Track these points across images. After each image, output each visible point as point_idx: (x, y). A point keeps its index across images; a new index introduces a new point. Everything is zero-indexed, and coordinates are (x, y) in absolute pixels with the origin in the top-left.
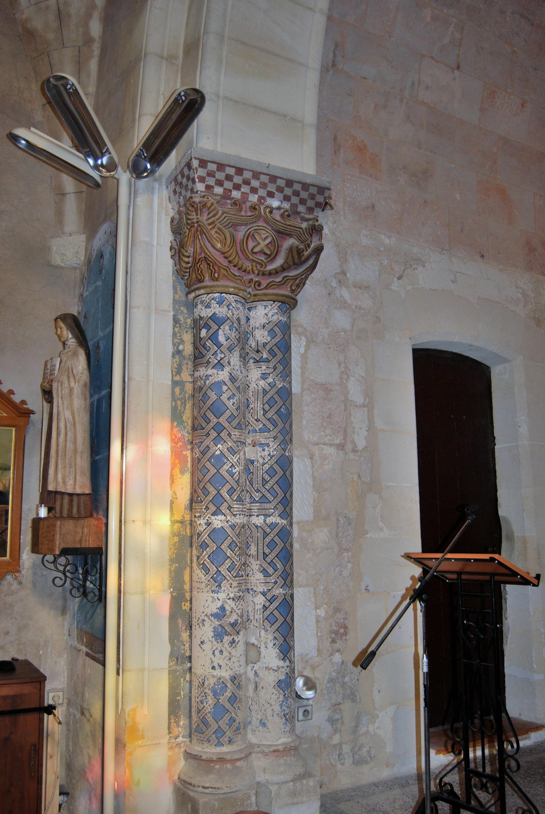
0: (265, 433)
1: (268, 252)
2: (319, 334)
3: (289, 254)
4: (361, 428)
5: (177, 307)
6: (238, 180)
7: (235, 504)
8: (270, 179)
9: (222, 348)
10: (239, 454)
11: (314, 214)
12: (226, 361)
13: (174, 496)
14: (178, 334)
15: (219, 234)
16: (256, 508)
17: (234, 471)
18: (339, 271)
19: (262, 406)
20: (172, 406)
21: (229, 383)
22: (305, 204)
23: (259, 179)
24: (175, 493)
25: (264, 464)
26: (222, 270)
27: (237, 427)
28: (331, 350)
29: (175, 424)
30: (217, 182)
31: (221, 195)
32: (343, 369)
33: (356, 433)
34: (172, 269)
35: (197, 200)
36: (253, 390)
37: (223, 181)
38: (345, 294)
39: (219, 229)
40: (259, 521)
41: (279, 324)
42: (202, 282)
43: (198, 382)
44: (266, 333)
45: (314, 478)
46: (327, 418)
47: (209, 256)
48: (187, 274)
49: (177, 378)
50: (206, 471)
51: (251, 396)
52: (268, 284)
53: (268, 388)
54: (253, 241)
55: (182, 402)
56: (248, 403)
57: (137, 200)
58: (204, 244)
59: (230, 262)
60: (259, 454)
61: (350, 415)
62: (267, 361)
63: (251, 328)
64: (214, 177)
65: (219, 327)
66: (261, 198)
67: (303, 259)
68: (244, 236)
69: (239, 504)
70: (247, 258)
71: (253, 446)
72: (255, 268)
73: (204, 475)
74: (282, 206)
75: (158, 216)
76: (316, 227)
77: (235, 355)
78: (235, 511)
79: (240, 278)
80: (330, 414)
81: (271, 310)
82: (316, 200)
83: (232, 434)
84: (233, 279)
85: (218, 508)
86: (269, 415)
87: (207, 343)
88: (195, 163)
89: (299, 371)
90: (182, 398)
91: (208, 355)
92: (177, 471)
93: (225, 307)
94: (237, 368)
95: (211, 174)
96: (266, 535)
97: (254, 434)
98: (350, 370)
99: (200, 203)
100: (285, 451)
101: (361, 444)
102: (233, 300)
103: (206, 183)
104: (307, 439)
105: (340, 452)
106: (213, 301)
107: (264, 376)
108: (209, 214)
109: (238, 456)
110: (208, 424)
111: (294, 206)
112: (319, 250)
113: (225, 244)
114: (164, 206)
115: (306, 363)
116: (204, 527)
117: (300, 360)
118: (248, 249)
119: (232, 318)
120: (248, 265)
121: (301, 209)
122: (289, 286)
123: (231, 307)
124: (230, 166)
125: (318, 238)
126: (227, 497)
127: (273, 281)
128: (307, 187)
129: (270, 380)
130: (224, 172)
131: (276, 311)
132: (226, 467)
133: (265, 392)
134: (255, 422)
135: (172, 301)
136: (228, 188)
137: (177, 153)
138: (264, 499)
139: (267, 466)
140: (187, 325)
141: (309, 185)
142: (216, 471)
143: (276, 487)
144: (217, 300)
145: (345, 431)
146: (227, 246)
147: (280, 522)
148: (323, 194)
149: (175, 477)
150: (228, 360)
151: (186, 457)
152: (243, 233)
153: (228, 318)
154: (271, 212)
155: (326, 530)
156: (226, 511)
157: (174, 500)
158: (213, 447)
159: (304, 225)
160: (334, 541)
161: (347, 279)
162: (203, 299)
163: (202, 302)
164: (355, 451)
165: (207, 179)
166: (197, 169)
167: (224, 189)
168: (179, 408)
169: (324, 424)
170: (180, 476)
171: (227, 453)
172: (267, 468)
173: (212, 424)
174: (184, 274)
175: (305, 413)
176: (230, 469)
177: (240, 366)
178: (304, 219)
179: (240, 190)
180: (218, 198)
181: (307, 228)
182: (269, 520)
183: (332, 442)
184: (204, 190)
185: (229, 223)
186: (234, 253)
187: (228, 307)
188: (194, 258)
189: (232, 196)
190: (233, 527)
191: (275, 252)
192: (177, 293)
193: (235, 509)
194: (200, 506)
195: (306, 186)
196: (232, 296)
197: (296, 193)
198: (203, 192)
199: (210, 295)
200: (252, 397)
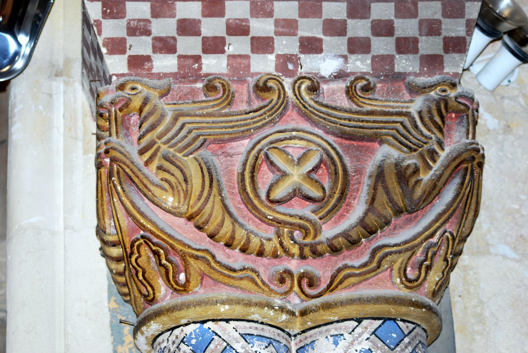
1: (316, 193)
11: (446, 70)
15: (168, 172)
22: (415, 50)
23: (270, 14)
26: (192, 261)
30: (158, 44)
31: (174, 75)
37: (174, 39)
39: (166, 158)
52: (333, 278)
54: (273, 172)
58: (132, 202)
64: (148, 33)
66: (285, 62)
67: (419, 192)
68: (245, 164)
70: (263, 218)
72: (287, 242)
74: (350, 68)
76: (452, 103)
81: (352, 343)
84: (226, 280)
102: (237, 335)
103: (129, 53)
106: (183, 347)
111: (383, 62)
118: (258, 196)
120: (264, 234)
121: (405, 64)
122: (395, 272)
125: (464, 130)
127: (346, 267)
130: (173, 16)
144: (193, 342)
148: (462, 16)
152: (240, 159)
159: (416, 105)
162: (163, 346)
166: (99, 24)
167: (180, 57)
178: (416, 90)
179: (223, 52)
181: (425, 109)
184: (125, 70)
185: (195, 139)
189: (205, 70)
196: (233, 324)
198: (123, 75)
199: (177, 332)
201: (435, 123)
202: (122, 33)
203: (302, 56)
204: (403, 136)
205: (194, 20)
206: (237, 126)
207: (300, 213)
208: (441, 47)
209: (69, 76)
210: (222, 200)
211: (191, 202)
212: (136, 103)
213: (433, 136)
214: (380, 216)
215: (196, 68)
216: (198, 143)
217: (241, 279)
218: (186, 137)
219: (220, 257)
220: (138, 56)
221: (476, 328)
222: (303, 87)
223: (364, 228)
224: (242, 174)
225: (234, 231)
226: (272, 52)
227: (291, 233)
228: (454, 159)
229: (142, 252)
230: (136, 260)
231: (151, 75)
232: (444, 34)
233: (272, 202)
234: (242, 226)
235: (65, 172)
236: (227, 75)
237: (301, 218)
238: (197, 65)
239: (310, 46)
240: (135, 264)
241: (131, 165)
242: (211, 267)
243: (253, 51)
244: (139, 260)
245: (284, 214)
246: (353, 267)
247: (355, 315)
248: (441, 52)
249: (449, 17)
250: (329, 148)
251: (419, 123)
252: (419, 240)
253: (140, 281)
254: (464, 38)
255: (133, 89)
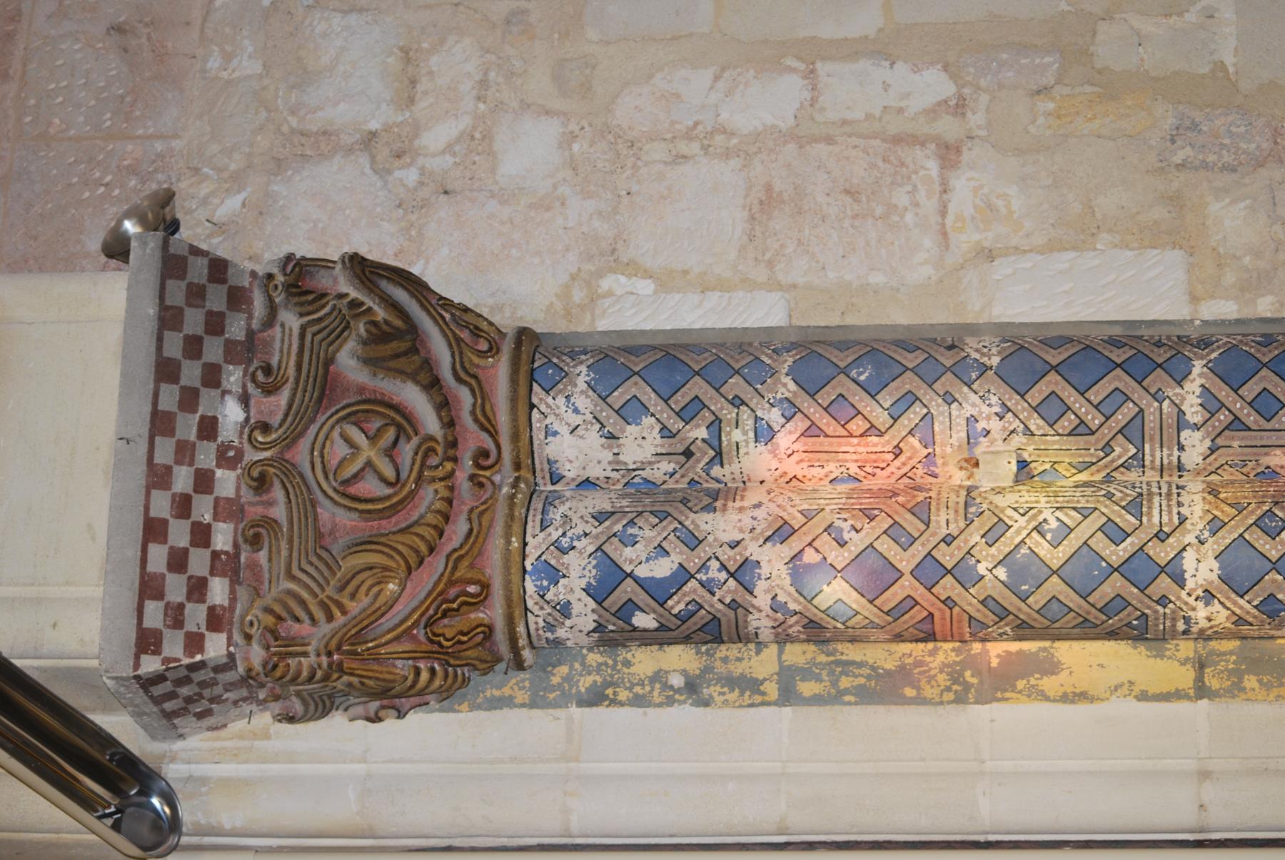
0: (936, 428)
1: (391, 433)
2: (585, 229)
3: (389, 369)
4: (886, 86)
5: (552, 696)
6: (179, 534)
7: (1149, 520)
8: (163, 434)
9: (692, 567)
10: (1002, 512)
11: (247, 284)
12: (731, 553)
13: (1125, 690)
14: (637, 689)
15: (359, 586)
16: (1158, 454)
17: (1054, 524)
18: (364, 160)
19: (855, 441)
20: (856, 704)
21: (795, 544)
22: (221, 315)
23: (168, 469)
24: (1116, 689)
25: (1029, 432)
26: (458, 574)
27: (925, 517)
28: (635, 188)
29: (910, 692)
30: (196, 596)
32: (695, 148)
33: (903, 104)
34: (437, 714)
35: (257, 655)
36: (805, 465)
38: (437, 137)
40: (1197, 443)
41: (599, 389)
42: (490, 629)
43: (790, 631)
44: (632, 430)
45: (1053, 247)
46: (857, 201)
47: (422, 615)
48: (459, 672)
49: (772, 689)
50: (1055, 605)
51: (823, 472)
53: (799, 424)
55: (842, 673)
56: (843, 481)
57: (227, 826)
59: (431, 550)
60: (1000, 446)
61: (845, 122)
62: (716, 424)
63: (615, 475)
64: (181, 607)
65: (630, 575)
66: (227, 458)
67: (398, 323)
68: (350, 509)
69: (1150, 508)
71: (977, 465)
72: (440, 473)
73: (1066, 610)
75: (277, 762)
76: (291, 279)
77: (708, 528)
78: (1171, 520)
79: (474, 516)
80: (847, 192)
83: (944, 532)
84: (481, 540)
85: (1163, 569)
86: (881, 419)
87: (675, 611)
88: (150, 665)
89: (714, 298)
90: (832, 673)
91: (712, 606)
92: (1049, 684)
93: (566, 559)
94: (747, 522)
95: (176, 616)
96: (1236, 424)
97: (939, 461)
98: (696, 124)
100: (985, 368)
101: (933, 85)
102: (542, 535)
103: (203, 630)
104: (928, 270)
105: (966, 156)
106: (548, 597)
107: (764, 434)
108: (297, 620)
109: (1010, 512)
110: (917, 603)
111: (235, 353)
112: (360, 267)
113: (386, 569)
114: (241, 744)
115: (686, 272)
116: (1217, 607)
117: (678, 297)
118: (389, 497)
119: (597, 537)
120: (429, 496)
121: (236, 328)
122: (481, 362)
123: (564, 540)
124: (144, 561)
125: (322, 271)
126: (1129, 545)
127: (473, 413)
129: (774, 416)
130: (163, 576)
131: (561, 400)
132: (1044, 549)
133: (813, 431)
134: (902, 458)
135: (536, 713)
137: (93, 711)
138: (1134, 431)
139: (1036, 423)
140: (606, 664)
141: (163, 308)
142: (1055, 579)
143: (1096, 395)
144: (545, 583)
145: (897, 140)
146: (392, 564)
147: (1199, 381)
149: (1069, 690)
150: (726, 547)
151: (1007, 658)
152: (340, 512)
153: (599, 548)
154: (265, 428)
155: (1215, 207)
156: (1171, 545)
157: (1137, 690)
158: (985, 588)
159: (291, 320)
160: (1247, 180)
161: (387, 128)
162: (542, 624)
163: (550, 627)
164: (959, 107)
165: (190, 626)
166: (166, 661)
167: (212, 574)
168: (862, 681)
169: (879, 211)
170: (1064, 675)
171: (1003, 547)
172: (1041, 422)
173: (919, 592)
174: (460, 678)
175: (848, 277)
176: (1049, 537)
177: (741, 509)
179: (209, 525)
180: (242, 593)
181: (298, 309)
182: (1194, 413)
183: (937, 187)
185: (320, 557)
186: (407, 539)
187: (564, 552)
188: (428, 655)
190: (1216, 526)
191: (392, 414)
193: (1165, 519)
194: (1157, 619)
195: (168, 319)
196: (529, 538)
197: (193, 347)
198: (229, 639)
199: (530, 604)
200: (827, 469)
201: (314, 300)
202: (180, 636)
203: (220, 439)
204: (330, 334)
205: (169, 554)
206: (306, 513)
207: (411, 454)
208: (220, 286)
209: (164, 756)
210: (394, 533)
211: (395, 565)
212: (270, 620)
213: (331, 303)
214: (421, 368)
216: (324, 555)
217: (480, 524)
218: (316, 568)
219: (456, 543)
221: (508, 314)
222: (260, 439)
223: (433, 387)
224: (362, 512)
225: (429, 525)
226: (214, 473)
227: (430, 468)
228: (362, 282)
229: (440, 631)
230: (448, 640)
231: (232, 608)
232: (204, 281)
234: (422, 517)
235: (293, 762)
236: (236, 524)
237: (416, 454)
240: (450, 643)
241: (349, 626)
242: (467, 553)
243: (211, 493)
244: (448, 636)
245: (411, 470)
246: (474, 405)
247: (526, 408)
248: (226, 287)
249: (185, 273)
250: (335, 418)
251: (315, 316)
252: (448, 332)
253: (470, 639)
254: (211, 260)
255: (251, 624)
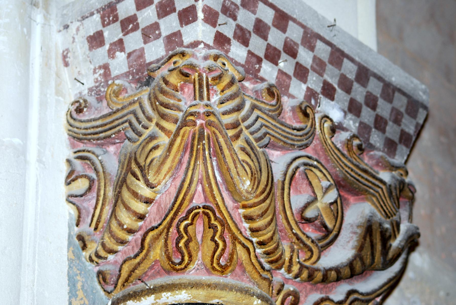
8: (332, 54)
26: (239, 247)
64: (234, 18)
67: (390, 255)
68: (285, 175)
82: (403, 126)
99: (210, 70)
128: (390, 91)
136: (256, 53)
165: (222, 18)
167: (250, 52)
181: (393, 185)
184: (211, 44)
189: (261, 74)
192: (76, 296)
215: (257, 68)
220: (222, 34)
233: (303, 218)
238: (258, 66)
239: (328, 91)
